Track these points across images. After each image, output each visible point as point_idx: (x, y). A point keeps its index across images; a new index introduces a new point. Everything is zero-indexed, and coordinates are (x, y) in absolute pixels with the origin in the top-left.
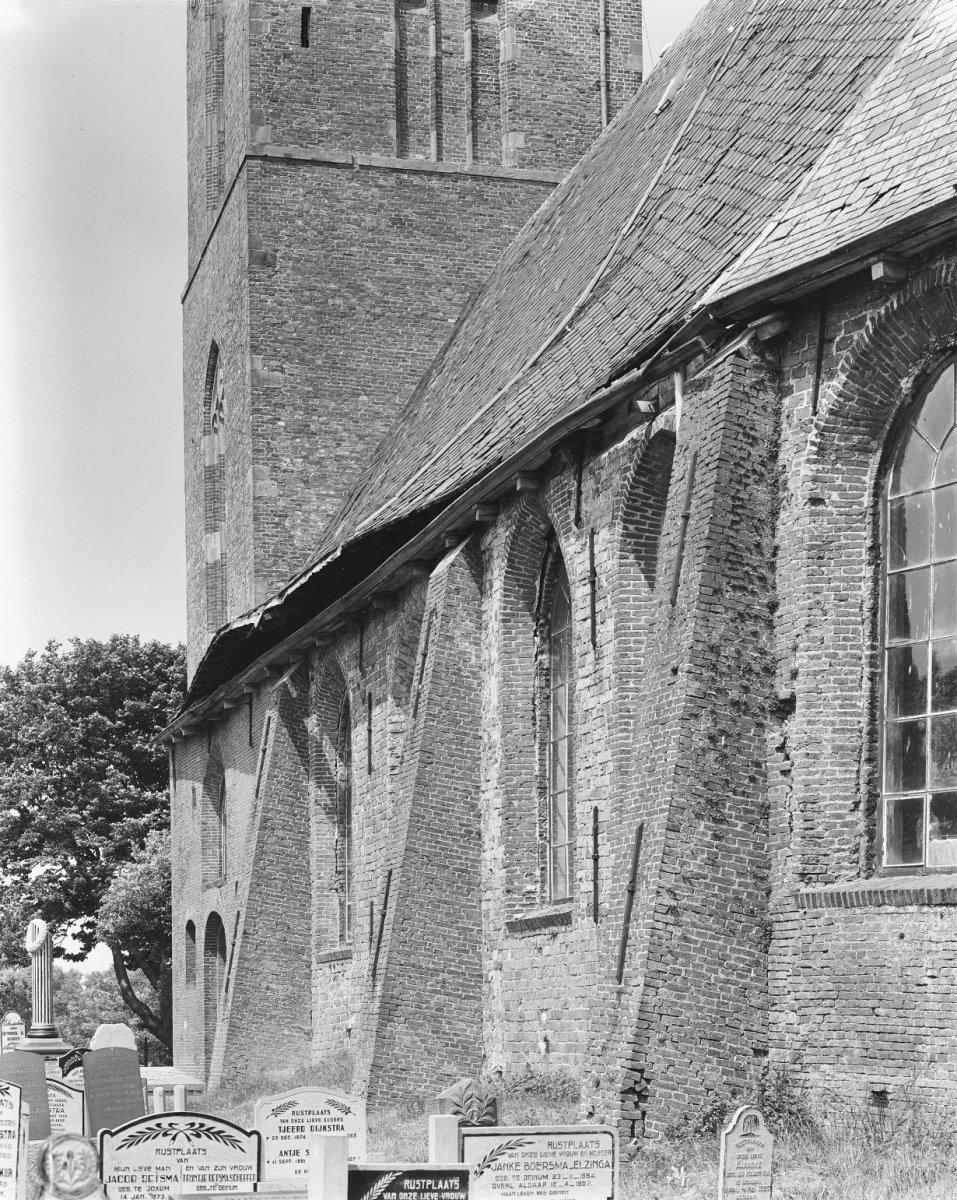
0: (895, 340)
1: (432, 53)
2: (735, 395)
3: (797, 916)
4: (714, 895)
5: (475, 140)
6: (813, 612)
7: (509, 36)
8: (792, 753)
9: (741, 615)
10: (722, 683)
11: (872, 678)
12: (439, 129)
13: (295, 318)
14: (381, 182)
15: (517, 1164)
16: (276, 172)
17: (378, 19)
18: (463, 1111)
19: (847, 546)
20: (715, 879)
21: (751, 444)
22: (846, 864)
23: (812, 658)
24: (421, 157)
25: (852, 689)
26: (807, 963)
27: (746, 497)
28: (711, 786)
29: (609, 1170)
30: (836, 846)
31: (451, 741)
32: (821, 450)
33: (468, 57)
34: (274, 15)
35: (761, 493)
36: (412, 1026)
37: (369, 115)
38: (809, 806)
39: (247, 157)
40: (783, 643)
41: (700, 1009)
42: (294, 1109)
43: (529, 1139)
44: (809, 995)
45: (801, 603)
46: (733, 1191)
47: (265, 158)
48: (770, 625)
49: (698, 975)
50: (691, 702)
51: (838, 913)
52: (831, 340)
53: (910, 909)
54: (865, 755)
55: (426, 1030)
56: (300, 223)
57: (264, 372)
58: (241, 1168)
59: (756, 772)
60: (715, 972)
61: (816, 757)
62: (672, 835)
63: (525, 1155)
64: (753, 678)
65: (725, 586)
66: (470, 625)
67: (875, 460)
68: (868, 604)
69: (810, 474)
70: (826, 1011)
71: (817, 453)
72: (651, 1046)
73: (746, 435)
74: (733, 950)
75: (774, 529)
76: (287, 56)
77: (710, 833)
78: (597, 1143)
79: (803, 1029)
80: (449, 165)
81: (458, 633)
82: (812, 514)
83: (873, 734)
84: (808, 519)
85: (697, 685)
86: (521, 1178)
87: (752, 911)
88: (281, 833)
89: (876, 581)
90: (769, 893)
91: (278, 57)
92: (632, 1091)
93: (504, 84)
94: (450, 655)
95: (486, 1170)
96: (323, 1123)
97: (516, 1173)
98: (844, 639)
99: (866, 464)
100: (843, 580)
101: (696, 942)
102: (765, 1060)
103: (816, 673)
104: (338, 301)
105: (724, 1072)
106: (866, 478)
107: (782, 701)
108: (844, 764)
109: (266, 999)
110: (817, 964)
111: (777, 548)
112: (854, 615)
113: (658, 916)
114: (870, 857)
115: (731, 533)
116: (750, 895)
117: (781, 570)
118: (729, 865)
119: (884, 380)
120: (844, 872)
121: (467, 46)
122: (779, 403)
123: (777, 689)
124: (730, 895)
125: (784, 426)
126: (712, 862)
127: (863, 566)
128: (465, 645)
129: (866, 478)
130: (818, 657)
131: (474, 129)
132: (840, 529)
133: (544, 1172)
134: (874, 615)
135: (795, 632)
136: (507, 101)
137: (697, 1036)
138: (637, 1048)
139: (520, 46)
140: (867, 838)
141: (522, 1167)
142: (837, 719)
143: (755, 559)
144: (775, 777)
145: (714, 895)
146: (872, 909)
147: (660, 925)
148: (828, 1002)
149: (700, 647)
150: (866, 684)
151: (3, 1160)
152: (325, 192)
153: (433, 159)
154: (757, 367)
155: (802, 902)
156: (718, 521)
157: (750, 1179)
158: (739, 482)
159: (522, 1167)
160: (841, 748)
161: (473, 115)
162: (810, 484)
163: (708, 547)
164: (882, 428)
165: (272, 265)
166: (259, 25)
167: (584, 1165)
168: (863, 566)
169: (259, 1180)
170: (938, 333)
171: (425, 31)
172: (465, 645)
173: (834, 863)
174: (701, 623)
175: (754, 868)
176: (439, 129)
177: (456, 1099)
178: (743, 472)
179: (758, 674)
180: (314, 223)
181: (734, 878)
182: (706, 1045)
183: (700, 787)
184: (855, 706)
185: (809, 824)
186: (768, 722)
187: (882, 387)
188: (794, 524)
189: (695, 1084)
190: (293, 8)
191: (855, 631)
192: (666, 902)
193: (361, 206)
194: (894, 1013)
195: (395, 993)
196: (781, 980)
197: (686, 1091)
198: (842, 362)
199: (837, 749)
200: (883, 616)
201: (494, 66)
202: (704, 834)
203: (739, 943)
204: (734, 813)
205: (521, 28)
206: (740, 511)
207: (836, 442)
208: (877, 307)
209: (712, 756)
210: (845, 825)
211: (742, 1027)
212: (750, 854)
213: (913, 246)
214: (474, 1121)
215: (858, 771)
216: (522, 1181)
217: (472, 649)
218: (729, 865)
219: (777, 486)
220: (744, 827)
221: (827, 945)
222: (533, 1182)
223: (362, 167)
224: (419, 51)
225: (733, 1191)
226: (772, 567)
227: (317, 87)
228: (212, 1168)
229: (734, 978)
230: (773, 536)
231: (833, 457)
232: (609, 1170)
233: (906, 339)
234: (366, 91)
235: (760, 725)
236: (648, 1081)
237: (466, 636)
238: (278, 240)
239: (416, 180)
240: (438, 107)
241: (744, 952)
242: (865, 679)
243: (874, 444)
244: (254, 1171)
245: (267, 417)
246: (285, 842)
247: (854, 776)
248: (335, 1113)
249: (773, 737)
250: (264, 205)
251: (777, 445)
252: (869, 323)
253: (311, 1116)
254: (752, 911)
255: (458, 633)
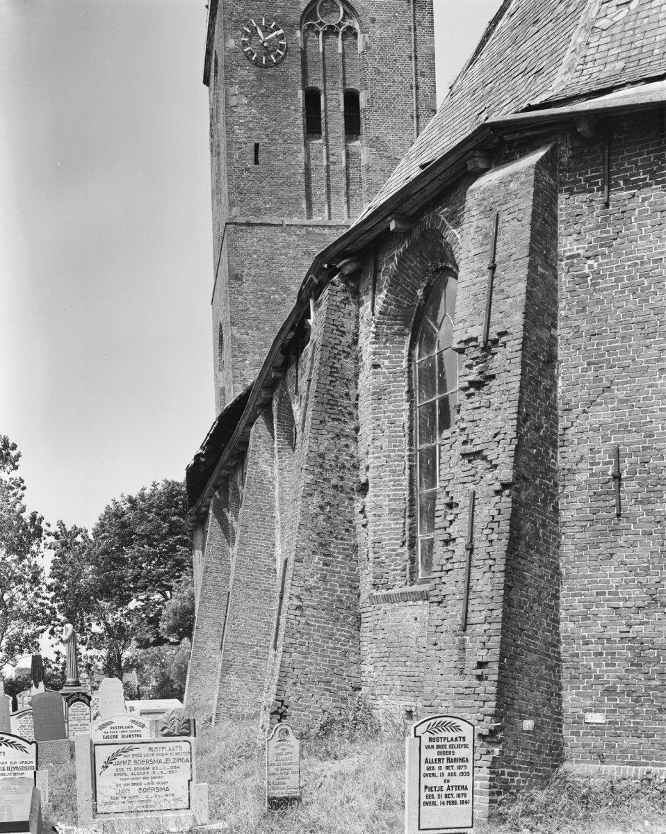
0: (410, 267)
1: (325, 163)
2: (330, 307)
3: (370, 609)
4: (325, 599)
5: (349, 207)
6: (376, 431)
7: (365, 152)
8: (368, 514)
9: (338, 435)
10: (327, 475)
11: (411, 468)
12: (329, 203)
13: (253, 306)
14: (298, 232)
15: (130, 761)
16: (242, 231)
17: (295, 147)
18: (169, 726)
19: (394, 391)
20: (325, 589)
21: (341, 336)
22: (398, 578)
23: (376, 458)
24: (320, 218)
25: (399, 475)
26: (376, 636)
27: (339, 366)
28: (321, 535)
29: (188, 764)
30: (393, 567)
31: (258, 520)
32: (377, 336)
33: (344, 164)
34: (240, 149)
35: (349, 363)
36: (240, 676)
37: (292, 198)
38: (377, 544)
39: (226, 224)
40: (362, 450)
41: (318, 665)
42: (112, 725)
43: (136, 746)
44: (377, 655)
45: (369, 427)
46: (274, 774)
47: (236, 223)
48: (356, 440)
49: (316, 645)
50: (308, 487)
51: (388, 606)
52: (380, 271)
53: (420, 602)
54: (407, 514)
55: (248, 678)
56: (255, 256)
57: (238, 335)
58: (26, 762)
59: (350, 526)
60: (327, 643)
61: (379, 516)
62: (298, 564)
63: (134, 755)
64: (346, 471)
65: (327, 419)
66: (267, 456)
67: (408, 340)
68: (407, 425)
69: (372, 350)
70: (385, 664)
71: (375, 338)
72: (288, 687)
73: (338, 330)
74: (338, 630)
75: (357, 384)
76: (247, 169)
77: (322, 562)
78: (180, 747)
79: (375, 675)
80: (334, 222)
81: (261, 460)
82: (374, 374)
83: (412, 501)
84: (371, 377)
85: (311, 477)
86: (133, 769)
87: (349, 607)
88: (215, 575)
89: (411, 411)
90: (359, 596)
91: (242, 170)
92: (276, 713)
93: (364, 177)
94: (256, 472)
95: (109, 765)
96: (129, 733)
97: (129, 767)
98: (394, 446)
99: (403, 342)
100: (392, 411)
101: (314, 626)
102: (359, 693)
103: (378, 467)
104: (276, 296)
105: (334, 701)
106: (404, 351)
107: (363, 485)
108: (395, 519)
109: (209, 663)
110: (380, 636)
111: (358, 395)
112: (399, 432)
113: (290, 612)
114: (412, 573)
115: (331, 388)
116: (347, 598)
117: (361, 409)
118: (334, 581)
119: (408, 291)
120: (397, 583)
121: (344, 158)
122: (358, 310)
123: (360, 478)
124: (335, 598)
125: (361, 324)
126: (324, 579)
127: (404, 403)
128: (264, 467)
129: (404, 351)
130: (380, 458)
131: (348, 202)
132: (390, 382)
133: (147, 766)
134: (411, 431)
135: (367, 443)
136: (365, 186)
137: (316, 680)
138: (279, 688)
139: (371, 156)
140: (410, 562)
141: (132, 763)
142: (390, 493)
143: (345, 402)
144: (360, 529)
145: (325, 599)
146: (402, 603)
147: (292, 617)
148: (385, 659)
149: (312, 455)
150: (407, 472)
151: (2, 756)
152: (268, 239)
153: (327, 219)
154: (344, 291)
155: (374, 600)
156: (322, 381)
157: (285, 767)
158: (335, 358)
159: (132, 763)
160: (394, 510)
161: (347, 194)
162: (372, 357)
163: (316, 397)
164: (410, 320)
165: (241, 279)
166: (232, 154)
167: (172, 761)
168: (404, 403)
169: (37, 769)
170: (432, 260)
171: (321, 152)
172: (264, 467)
173: (391, 578)
174: (313, 441)
175: (350, 582)
176: (329, 203)
177: (165, 720)
178: (336, 352)
179: (349, 469)
180: (262, 256)
181: (337, 588)
182: (323, 686)
183: (315, 536)
184: (401, 485)
185: (377, 555)
186: (356, 497)
187: (407, 296)
188: (366, 381)
189: (316, 708)
190: (250, 144)
191: (400, 441)
192: (295, 603)
193: (288, 246)
194: (414, 664)
195: (230, 658)
196: (366, 647)
197: (310, 712)
198: (385, 283)
199: (392, 511)
200: (416, 431)
201: (358, 168)
202: (318, 563)
203: (341, 626)
204: (336, 551)
205: (372, 146)
206: (335, 375)
207: (385, 330)
208: (398, 248)
209: (321, 518)
210: (398, 555)
211: (345, 674)
212: (347, 574)
213: (410, 207)
214: (175, 733)
215: (404, 523)
216: (133, 771)
217: (269, 469)
218: (334, 581)
219: (357, 359)
220: (343, 558)
221: (384, 625)
222: (140, 771)
223: (287, 225)
224: (318, 163)
225: (274, 774)
226: (356, 406)
227: (263, 185)
228: (9, 763)
229: (339, 646)
230: (356, 388)
231: (384, 340)
232: (188, 764)
233: (416, 266)
234: (289, 186)
235: (351, 499)
236: (287, 707)
237: (266, 461)
238: (243, 266)
239: (317, 230)
240: (328, 192)
241: (345, 631)
242: (407, 469)
243: (407, 331)
244: (34, 764)
245: (240, 359)
246: (218, 579)
247: (401, 526)
248: (136, 727)
249: (358, 506)
250: (236, 248)
251: (357, 336)
252: (396, 258)
253: (122, 730)
254: (349, 607)
255: (261, 460)
